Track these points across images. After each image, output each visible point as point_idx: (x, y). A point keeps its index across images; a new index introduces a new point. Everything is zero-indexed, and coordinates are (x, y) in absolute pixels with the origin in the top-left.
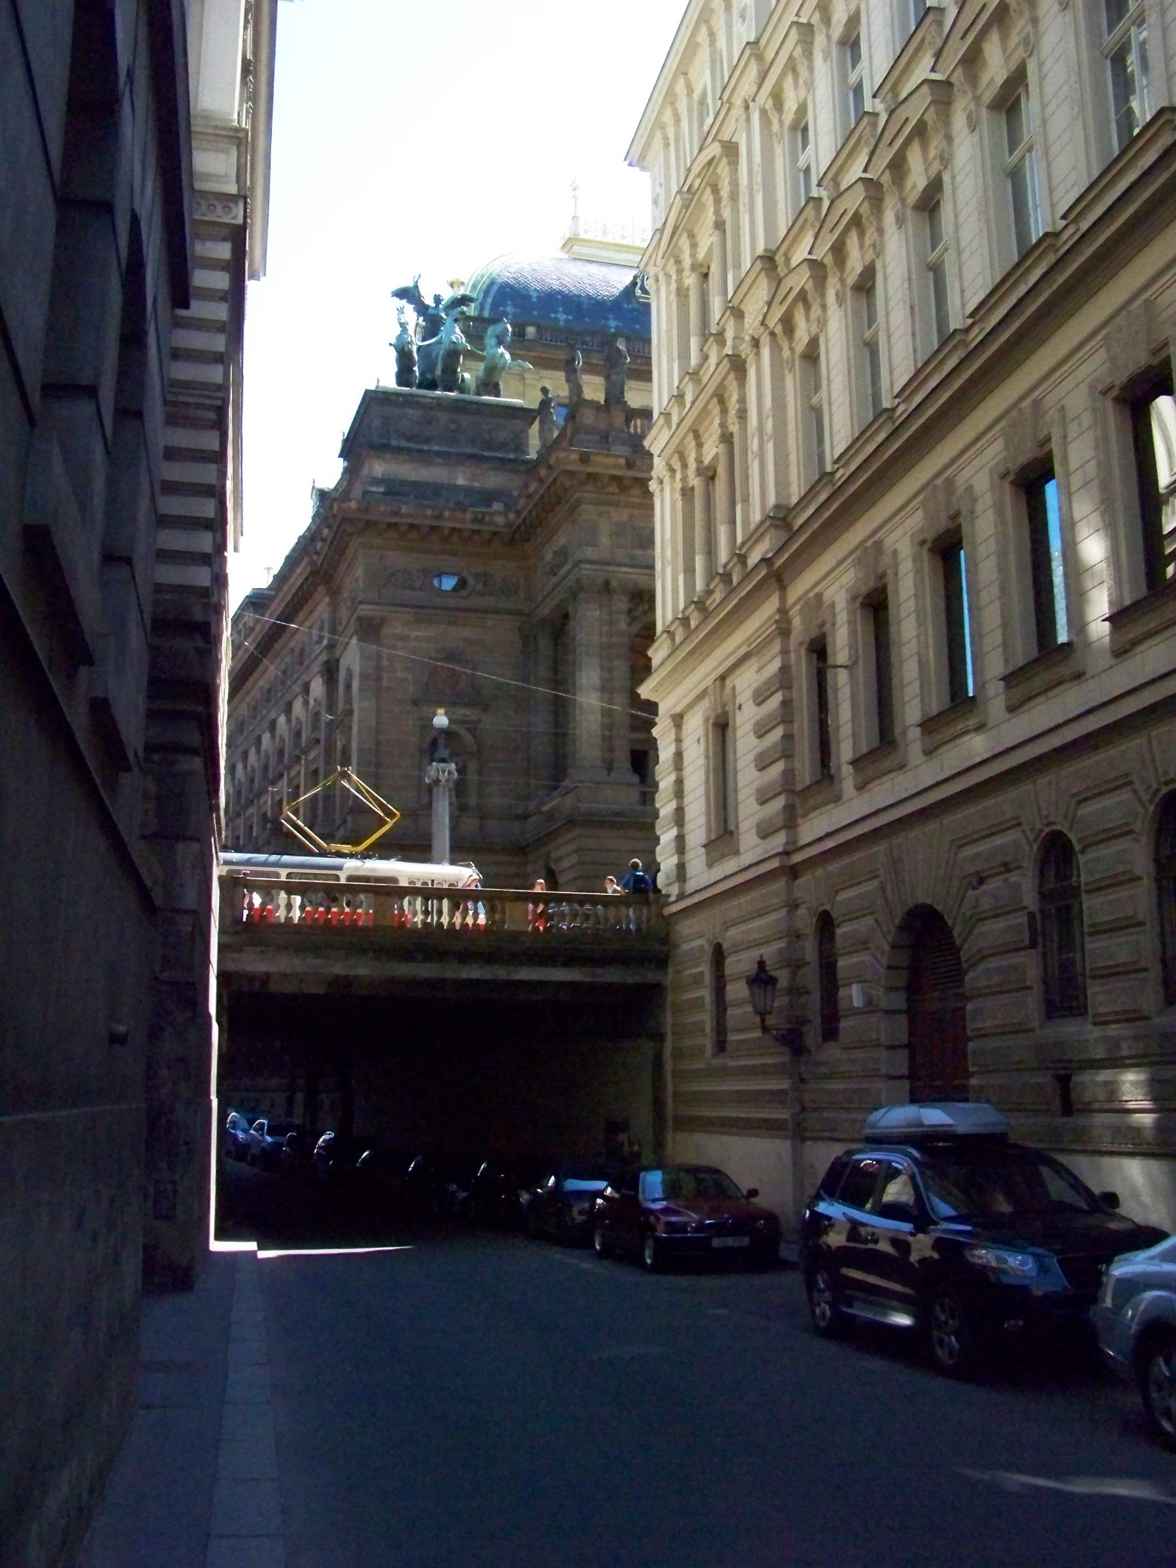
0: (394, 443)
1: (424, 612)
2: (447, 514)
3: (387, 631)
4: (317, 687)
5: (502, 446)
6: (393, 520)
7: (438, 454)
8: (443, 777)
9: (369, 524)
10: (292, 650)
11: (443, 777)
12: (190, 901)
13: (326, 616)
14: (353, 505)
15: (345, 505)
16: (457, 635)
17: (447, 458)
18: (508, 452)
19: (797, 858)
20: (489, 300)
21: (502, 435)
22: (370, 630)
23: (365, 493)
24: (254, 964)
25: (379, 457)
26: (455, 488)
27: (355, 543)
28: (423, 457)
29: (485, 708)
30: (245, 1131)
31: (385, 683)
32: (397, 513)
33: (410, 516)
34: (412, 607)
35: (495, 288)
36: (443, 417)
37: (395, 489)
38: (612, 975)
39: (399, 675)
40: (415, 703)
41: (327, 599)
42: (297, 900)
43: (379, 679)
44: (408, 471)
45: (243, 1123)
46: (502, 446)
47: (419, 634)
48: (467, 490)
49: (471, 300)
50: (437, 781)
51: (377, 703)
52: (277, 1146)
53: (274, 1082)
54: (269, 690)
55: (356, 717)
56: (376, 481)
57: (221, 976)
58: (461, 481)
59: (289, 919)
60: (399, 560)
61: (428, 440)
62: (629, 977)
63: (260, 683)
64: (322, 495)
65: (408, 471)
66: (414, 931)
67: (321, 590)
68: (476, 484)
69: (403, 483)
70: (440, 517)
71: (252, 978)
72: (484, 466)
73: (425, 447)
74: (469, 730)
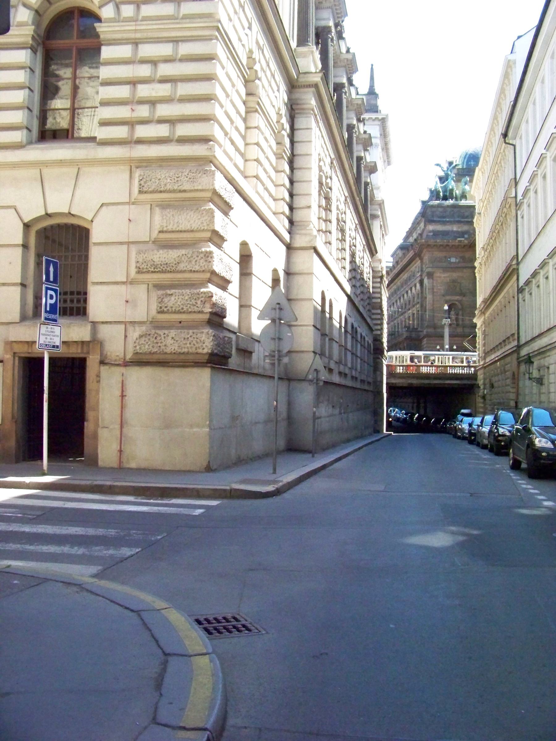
0: (435, 219)
1: (445, 269)
2: (450, 241)
3: (435, 275)
4: (418, 286)
5: (467, 217)
6: (435, 244)
7: (448, 222)
8: (447, 323)
9: (429, 245)
10: (412, 271)
11: (447, 323)
12: (379, 379)
13: (420, 265)
14: (423, 241)
15: (421, 241)
16: (455, 275)
17: (450, 223)
18: (469, 219)
19: (485, 365)
20: (466, 160)
21: (466, 214)
22: (430, 275)
23: (427, 235)
24: (393, 381)
25: (430, 224)
26: (452, 231)
27: (425, 251)
28: (444, 223)
29: (464, 296)
30: (399, 414)
31: (435, 290)
32: (436, 242)
33: (439, 242)
34: (442, 268)
35: (467, 156)
36: (449, 210)
37: (436, 234)
38: (465, 382)
39: (439, 288)
40: (443, 296)
41: (420, 261)
42: (401, 368)
43: (433, 289)
44: (439, 228)
45: (399, 412)
46: (467, 217)
47: (444, 275)
48: (457, 232)
49: (459, 165)
50: (445, 324)
51: (433, 296)
52: (406, 418)
53: (410, 400)
54: (406, 280)
55: (427, 299)
56: (430, 232)
57: (387, 384)
58: (455, 229)
59: (400, 372)
60: (438, 254)
61: (444, 217)
62: (469, 382)
63: (403, 277)
64: (424, 203)
65: (439, 228)
66: (425, 373)
67: (418, 259)
68: (460, 230)
69: (438, 231)
70: (449, 242)
71: (393, 383)
72: (462, 224)
73: (444, 220)
74: (459, 302)
